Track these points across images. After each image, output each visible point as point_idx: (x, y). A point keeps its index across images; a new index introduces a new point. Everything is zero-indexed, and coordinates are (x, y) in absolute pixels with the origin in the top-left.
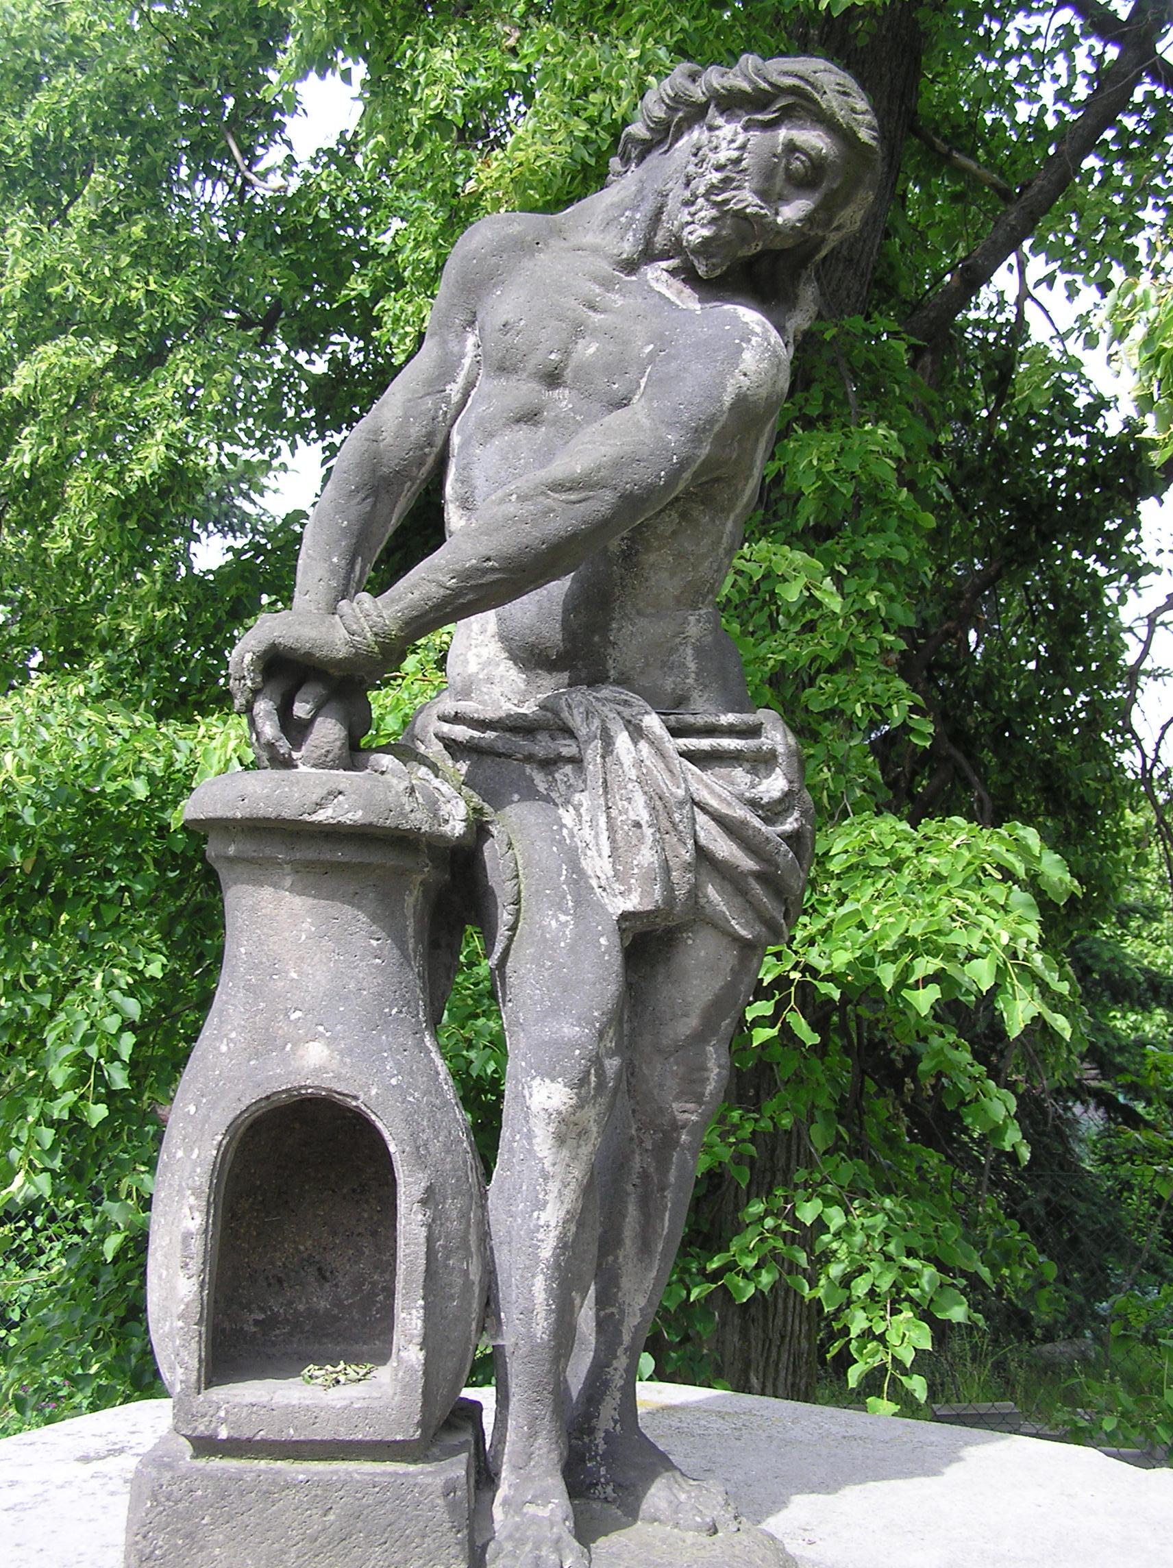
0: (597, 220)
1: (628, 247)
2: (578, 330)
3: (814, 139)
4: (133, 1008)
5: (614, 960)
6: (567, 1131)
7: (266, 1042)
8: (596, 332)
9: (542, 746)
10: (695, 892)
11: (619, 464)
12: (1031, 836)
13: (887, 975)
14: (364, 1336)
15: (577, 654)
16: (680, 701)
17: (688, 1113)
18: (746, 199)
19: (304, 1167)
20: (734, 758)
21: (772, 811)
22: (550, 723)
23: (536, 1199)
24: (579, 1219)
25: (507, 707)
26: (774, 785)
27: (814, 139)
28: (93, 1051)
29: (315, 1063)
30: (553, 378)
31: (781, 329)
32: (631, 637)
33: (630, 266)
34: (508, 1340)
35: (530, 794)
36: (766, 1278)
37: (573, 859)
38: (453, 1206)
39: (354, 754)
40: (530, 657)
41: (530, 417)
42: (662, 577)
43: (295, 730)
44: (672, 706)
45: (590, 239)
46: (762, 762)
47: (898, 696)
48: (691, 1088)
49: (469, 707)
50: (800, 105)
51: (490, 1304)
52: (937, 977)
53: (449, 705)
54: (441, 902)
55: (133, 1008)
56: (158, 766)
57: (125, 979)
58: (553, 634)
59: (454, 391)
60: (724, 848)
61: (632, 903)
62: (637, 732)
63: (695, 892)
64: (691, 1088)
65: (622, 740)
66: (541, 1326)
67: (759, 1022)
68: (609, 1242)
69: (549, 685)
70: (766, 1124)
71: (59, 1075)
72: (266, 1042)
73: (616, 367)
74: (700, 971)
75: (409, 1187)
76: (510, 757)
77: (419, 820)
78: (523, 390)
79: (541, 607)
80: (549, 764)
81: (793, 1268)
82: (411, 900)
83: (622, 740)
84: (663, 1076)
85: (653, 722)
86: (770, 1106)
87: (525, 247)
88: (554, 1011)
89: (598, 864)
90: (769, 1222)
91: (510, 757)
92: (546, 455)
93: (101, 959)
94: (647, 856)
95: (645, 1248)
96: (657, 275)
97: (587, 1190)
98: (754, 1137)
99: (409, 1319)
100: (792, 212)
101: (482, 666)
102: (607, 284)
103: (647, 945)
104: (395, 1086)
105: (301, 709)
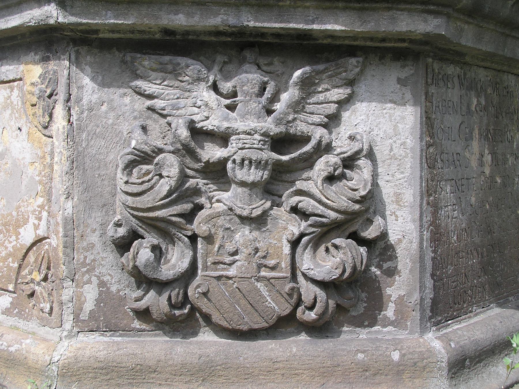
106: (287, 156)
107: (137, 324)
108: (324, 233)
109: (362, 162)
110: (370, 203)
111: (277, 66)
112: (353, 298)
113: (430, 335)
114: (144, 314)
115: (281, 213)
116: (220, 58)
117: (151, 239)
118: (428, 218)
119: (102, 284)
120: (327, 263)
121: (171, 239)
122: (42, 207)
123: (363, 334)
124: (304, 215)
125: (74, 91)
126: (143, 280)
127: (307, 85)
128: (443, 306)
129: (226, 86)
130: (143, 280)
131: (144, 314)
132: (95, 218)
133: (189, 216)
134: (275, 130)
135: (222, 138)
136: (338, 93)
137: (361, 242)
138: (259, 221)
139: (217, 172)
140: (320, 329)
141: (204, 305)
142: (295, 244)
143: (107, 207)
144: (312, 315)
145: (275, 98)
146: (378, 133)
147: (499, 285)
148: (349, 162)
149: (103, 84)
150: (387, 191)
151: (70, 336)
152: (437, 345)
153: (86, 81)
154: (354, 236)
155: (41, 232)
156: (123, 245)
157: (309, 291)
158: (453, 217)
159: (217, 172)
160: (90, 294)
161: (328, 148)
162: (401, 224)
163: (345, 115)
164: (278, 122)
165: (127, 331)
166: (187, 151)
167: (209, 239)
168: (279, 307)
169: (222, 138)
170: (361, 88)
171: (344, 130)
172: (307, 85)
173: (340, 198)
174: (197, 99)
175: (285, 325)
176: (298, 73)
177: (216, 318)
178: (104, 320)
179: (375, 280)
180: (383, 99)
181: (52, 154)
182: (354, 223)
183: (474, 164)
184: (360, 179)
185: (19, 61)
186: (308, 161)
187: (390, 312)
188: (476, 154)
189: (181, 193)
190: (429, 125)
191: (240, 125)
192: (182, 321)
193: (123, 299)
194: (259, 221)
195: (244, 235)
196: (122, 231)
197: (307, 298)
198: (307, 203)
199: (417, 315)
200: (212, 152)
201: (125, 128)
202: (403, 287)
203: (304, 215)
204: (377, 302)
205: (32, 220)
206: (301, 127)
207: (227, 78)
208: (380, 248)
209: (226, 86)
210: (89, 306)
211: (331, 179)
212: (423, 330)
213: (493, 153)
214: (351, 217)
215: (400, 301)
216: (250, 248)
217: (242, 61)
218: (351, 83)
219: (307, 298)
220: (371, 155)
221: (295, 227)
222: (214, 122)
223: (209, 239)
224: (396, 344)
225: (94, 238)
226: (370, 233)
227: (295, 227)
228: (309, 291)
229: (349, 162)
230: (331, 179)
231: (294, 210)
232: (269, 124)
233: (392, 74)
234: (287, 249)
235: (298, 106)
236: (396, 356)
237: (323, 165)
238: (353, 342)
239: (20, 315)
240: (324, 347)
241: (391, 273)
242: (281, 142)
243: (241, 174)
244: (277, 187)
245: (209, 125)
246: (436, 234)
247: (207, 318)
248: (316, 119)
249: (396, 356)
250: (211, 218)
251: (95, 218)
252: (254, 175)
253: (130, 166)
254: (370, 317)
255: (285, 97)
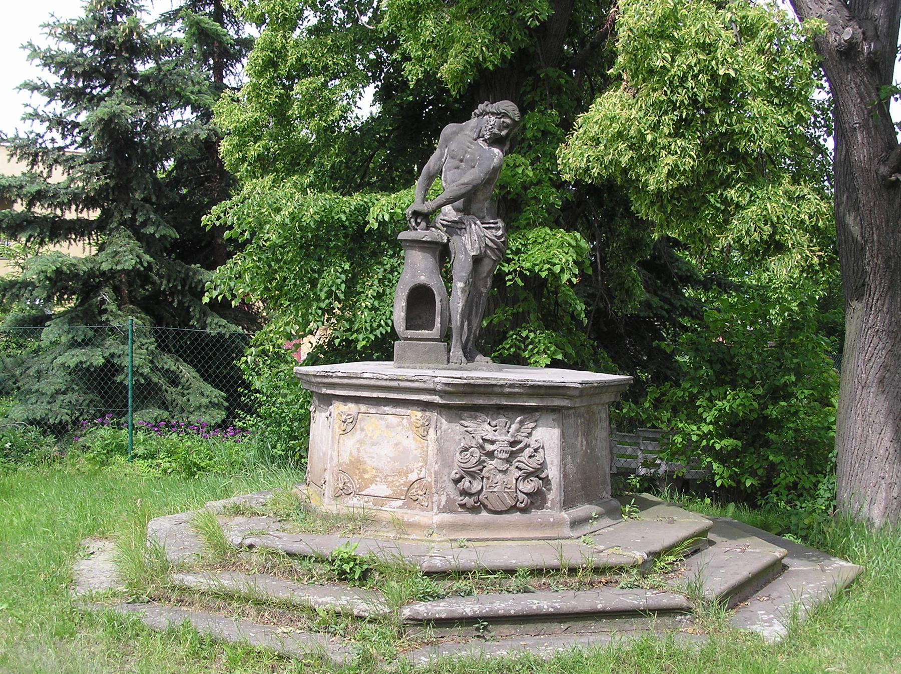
0: (469, 128)
1: (475, 136)
2: (466, 152)
3: (508, 121)
4: (343, 277)
5: (471, 263)
6: (463, 291)
7: (414, 276)
8: (469, 153)
9: (459, 226)
10: (485, 251)
11: (473, 180)
12: (578, 235)
13: (537, 269)
14: (430, 326)
15: (466, 210)
16: (484, 218)
17: (484, 290)
18: (496, 131)
19: (420, 298)
20: (493, 228)
21: (499, 238)
22: (461, 222)
23: (458, 303)
24: (465, 306)
25: (454, 219)
26: (500, 233)
27: (508, 121)
28: (334, 289)
29: (423, 279)
30: (461, 161)
31: (502, 151)
32: (475, 207)
33: (475, 140)
34: (452, 326)
35: (457, 234)
36: (513, 350)
37: (464, 246)
38: (445, 303)
39: (427, 228)
40: (457, 210)
41: (458, 168)
42: (480, 196)
43: (418, 224)
44: (481, 219)
45: (468, 133)
46: (498, 229)
47: (553, 193)
48: (485, 286)
49: (446, 218)
50: (505, 115)
51: (450, 321)
52: (549, 269)
53: (443, 217)
54: (442, 253)
55: (343, 277)
56: (347, 210)
57: (340, 270)
58: (461, 206)
59: (443, 160)
60: (490, 244)
61: (474, 254)
62: (475, 224)
63: (485, 251)
64: (485, 286)
65: (473, 225)
66: (459, 324)
67: (509, 280)
68: (470, 314)
69: (460, 215)
70: (515, 311)
71: (323, 295)
72: (414, 276)
73: (473, 160)
74: (486, 265)
75: (438, 299)
76: (453, 228)
77: (439, 240)
78: (457, 162)
79: (459, 203)
80: (461, 229)
81: (520, 348)
82: (437, 253)
83: (473, 225)
84: (480, 284)
85: (478, 222)
86: (516, 306)
87: (456, 133)
88: (461, 271)
89: (469, 247)
90: (514, 337)
91: (453, 228)
92: (460, 176)
93: (329, 265)
94: (477, 246)
95: (477, 315)
96: (480, 141)
97: (466, 301)
98: (513, 314)
99: (438, 319)
100: (503, 133)
101: (449, 213)
102: (471, 143)
103: (477, 261)
104: (435, 283)
105: (419, 221)
106: (515, 449)
107: (460, 510)
108: (527, 476)
109: (540, 450)
110: (543, 466)
111: (510, 415)
112: (537, 499)
113: (563, 513)
114: (463, 506)
115: (513, 468)
116: (491, 413)
117: (468, 479)
118: (562, 469)
119: (448, 495)
120: (529, 486)
121: (474, 478)
122: (422, 466)
123: (539, 512)
124: (520, 469)
125: (439, 424)
126: (464, 493)
127: (521, 423)
128: (568, 503)
129: (493, 423)
130: (464, 493)
131: (463, 506)
132: (446, 471)
133: (481, 470)
134: (512, 440)
135: (492, 442)
136: (532, 425)
137: (540, 479)
138: (505, 472)
139: (491, 455)
140: (524, 511)
141: (486, 502)
142: (517, 480)
143: (450, 467)
144: (523, 505)
145: (510, 427)
146: (545, 439)
147: (589, 496)
148: (536, 450)
149: (449, 422)
150: (548, 460)
151: (436, 514)
152: (566, 516)
153: (444, 421)
154: (537, 476)
155: (421, 476)
156: (457, 481)
157: (521, 496)
158: (571, 468)
159: (491, 455)
160: (444, 499)
161: (529, 446)
162: (553, 472)
163: (534, 432)
164: (512, 436)
165: (456, 512)
166: (482, 447)
167: (488, 478)
168: (511, 502)
169: (492, 442)
170: (540, 423)
171: (533, 438)
172: (521, 423)
173: (534, 463)
174: (484, 428)
175: (513, 509)
176: (519, 419)
177: (490, 506)
178: (448, 508)
179: (544, 492)
180: (547, 426)
181: (427, 447)
182: (537, 473)
183: (579, 446)
184: (539, 457)
185: (407, 408)
186: (522, 450)
187: (549, 504)
188: (580, 443)
189: (480, 462)
190: (563, 435)
191: (499, 438)
192: (474, 510)
193: (456, 500)
194: (505, 472)
195: (500, 476)
196: (458, 476)
197: (521, 499)
198: (521, 465)
199: (558, 505)
200: (489, 447)
201: (457, 438)
202: (554, 495)
203: (520, 469)
204: (544, 500)
205: (416, 471)
206: (519, 438)
207: (493, 420)
208: (546, 481)
209: (493, 423)
210: (443, 503)
211: (530, 457)
212: (561, 511)
213: (586, 440)
214: (537, 470)
215: (553, 500)
216: (502, 482)
217: (499, 414)
218: (536, 421)
219: (521, 499)
220: (543, 448)
221: (518, 473)
222: (489, 437)
223: (488, 478)
224: (552, 516)
225: (446, 478)
226: (543, 475)
227: (518, 473)
228: (521, 496)
229: (536, 450)
230: (530, 457)
231: (517, 467)
232: (509, 438)
233: (551, 417)
234: (514, 481)
235: (518, 430)
236: (552, 520)
237: (527, 452)
238: (536, 515)
239: (408, 508)
240: (526, 516)
241: (549, 490)
242: (513, 444)
243: (500, 456)
244: (511, 459)
245: (487, 437)
246: (565, 475)
247: (485, 507)
248: (524, 434)
249: (552, 520)
250: (489, 471)
251: (446, 471)
252: (505, 456)
253: (462, 452)
254: (541, 507)
255: (513, 426)
